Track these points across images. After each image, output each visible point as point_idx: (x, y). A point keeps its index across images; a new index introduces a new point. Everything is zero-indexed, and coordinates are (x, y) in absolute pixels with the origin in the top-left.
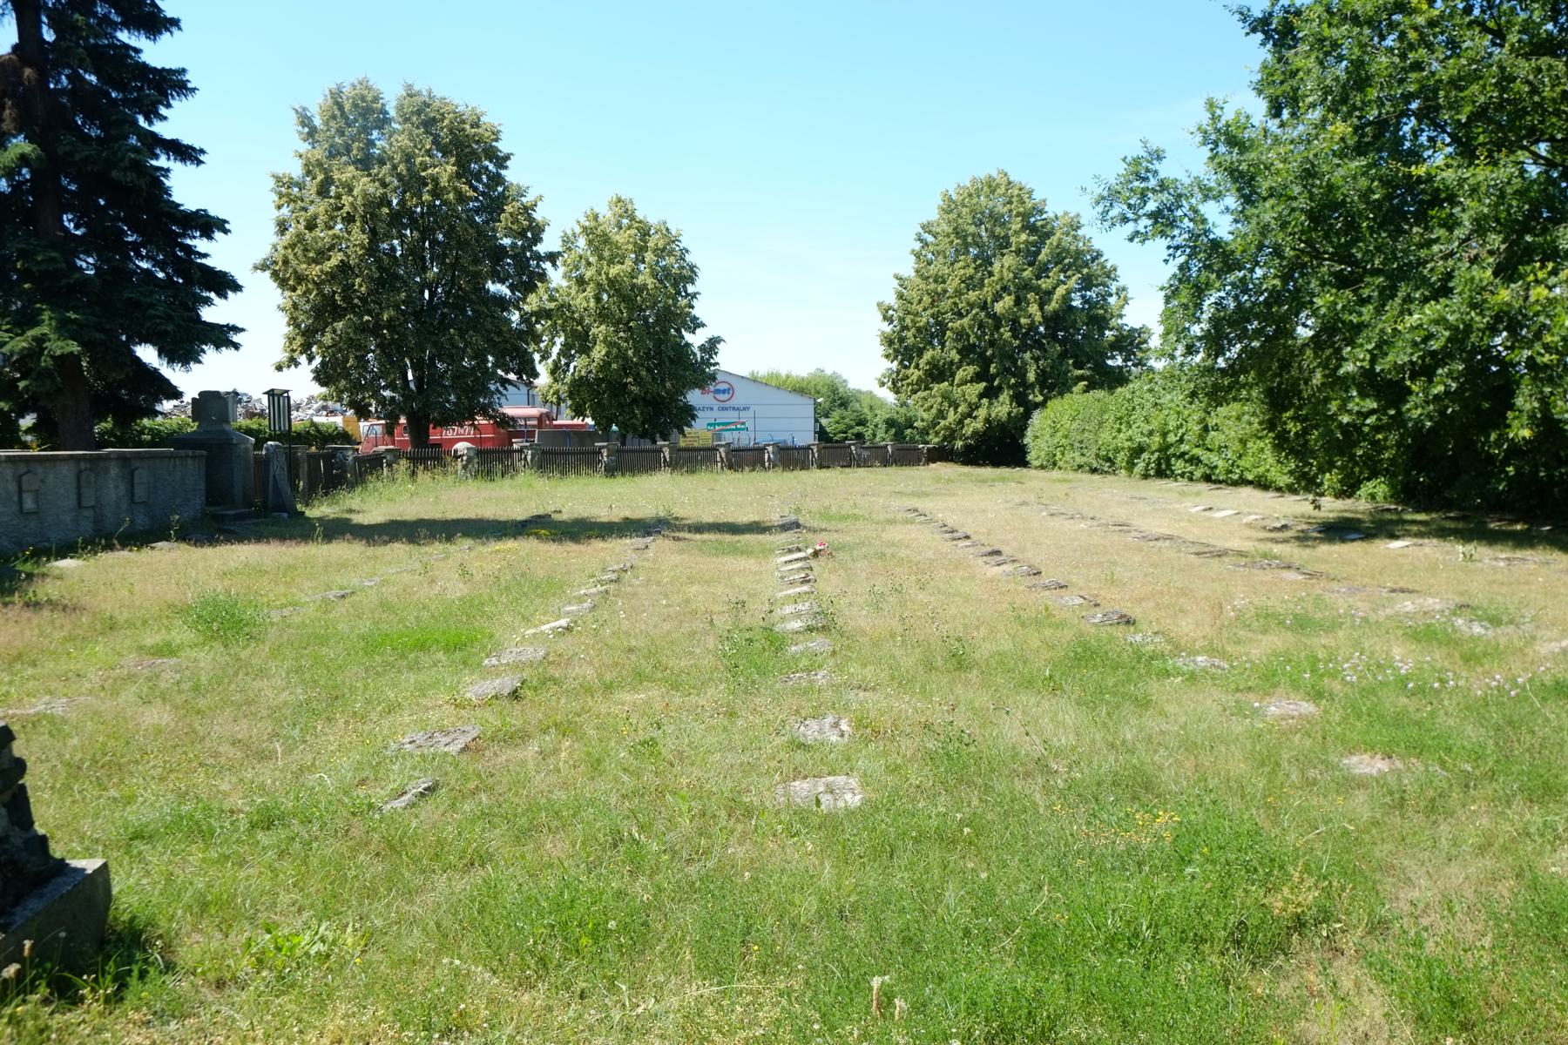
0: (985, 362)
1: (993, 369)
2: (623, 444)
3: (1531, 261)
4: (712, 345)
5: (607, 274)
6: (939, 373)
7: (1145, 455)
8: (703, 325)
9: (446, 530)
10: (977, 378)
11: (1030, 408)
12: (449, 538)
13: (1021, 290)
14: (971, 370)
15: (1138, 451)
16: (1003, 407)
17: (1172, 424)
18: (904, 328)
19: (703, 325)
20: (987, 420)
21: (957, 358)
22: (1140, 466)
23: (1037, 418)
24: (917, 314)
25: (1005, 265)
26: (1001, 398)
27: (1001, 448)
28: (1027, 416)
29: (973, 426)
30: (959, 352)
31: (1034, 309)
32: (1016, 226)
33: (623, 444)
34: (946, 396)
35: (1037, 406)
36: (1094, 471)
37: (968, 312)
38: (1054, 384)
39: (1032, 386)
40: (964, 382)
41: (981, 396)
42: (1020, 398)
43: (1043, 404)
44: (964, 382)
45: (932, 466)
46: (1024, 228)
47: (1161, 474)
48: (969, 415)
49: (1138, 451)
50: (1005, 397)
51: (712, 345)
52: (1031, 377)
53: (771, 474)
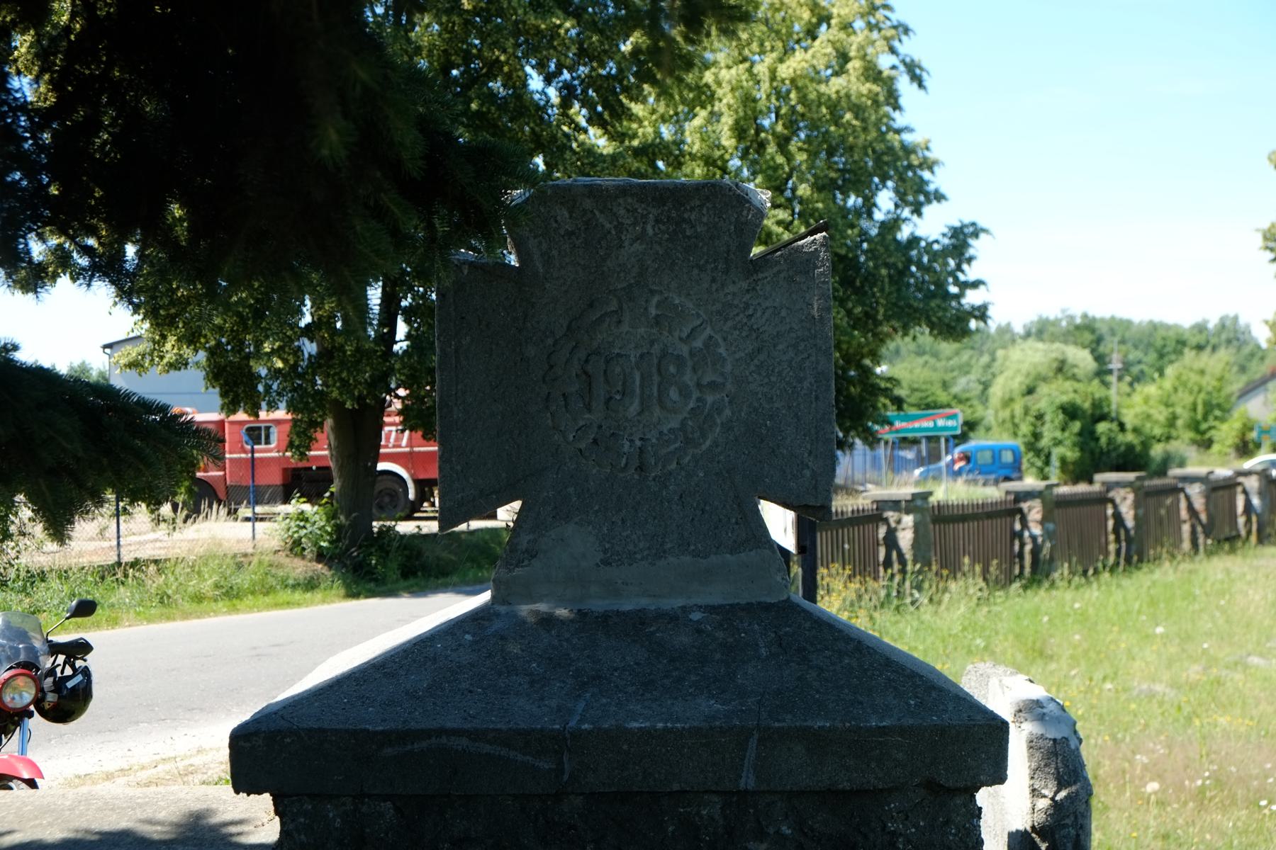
4: (961, 239)
8: (939, 197)
19: (939, 197)
51: (961, 239)
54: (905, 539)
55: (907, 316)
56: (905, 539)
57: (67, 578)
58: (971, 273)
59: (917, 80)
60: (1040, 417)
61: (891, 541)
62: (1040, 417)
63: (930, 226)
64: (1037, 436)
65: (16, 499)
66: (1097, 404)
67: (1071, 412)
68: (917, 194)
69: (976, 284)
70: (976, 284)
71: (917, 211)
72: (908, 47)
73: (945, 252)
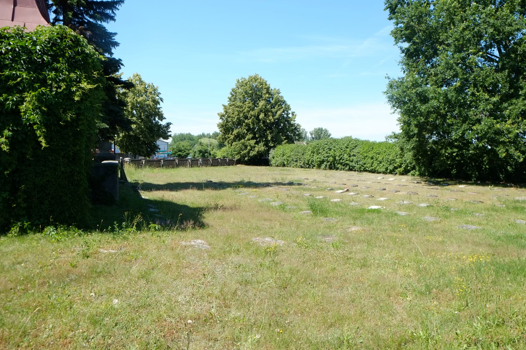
0: (255, 134)
1: (257, 136)
2: (135, 158)
3: (500, 99)
4: (168, 125)
5: (136, 100)
6: (239, 137)
7: (325, 163)
8: (165, 118)
9: (235, 185)
10: (253, 138)
11: (270, 148)
12: (224, 188)
13: (266, 112)
14: (251, 136)
15: (323, 162)
16: (261, 147)
17: (338, 154)
18: (227, 122)
19: (165, 118)
20: (258, 152)
21: (246, 132)
22: (323, 166)
23: (272, 152)
24: (233, 117)
25: (262, 103)
26: (260, 144)
27: (261, 160)
28: (268, 151)
29: (252, 154)
30: (247, 130)
31: (271, 118)
32: (264, 92)
33: (135, 158)
34: (243, 144)
35: (271, 147)
36: (302, 167)
37: (251, 118)
38: (277, 141)
39: (269, 141)
40: (249, 140)
41: (255, 144)
42: (266, 145)
43: (274, 147)
44: (249, 140)
45: (238, 165)
46: (267, 93)
47: (331, 168)
48: (251, 150)
49: (323, 162)
50: (261, 144)
51: (168, 125)
52: (269, 138)
53: (200, 168)
54: (144, 163)
55: (159, 136)
56: (144, 163)
57: (442, 231)
58: (170, 130)
59: (162, 101)
60: (195, 152)
61: (142, 163)
62: (195, 152)
63: (163, 123)
64: (195, 156)
65: (417, 129)
66: (206, 150)
67: (200, 151)
68: (162, 118)
69: (170, 132)
70: (170, 132)
71: (162, 120)
72: (160, 96)
73: (166, 127)
